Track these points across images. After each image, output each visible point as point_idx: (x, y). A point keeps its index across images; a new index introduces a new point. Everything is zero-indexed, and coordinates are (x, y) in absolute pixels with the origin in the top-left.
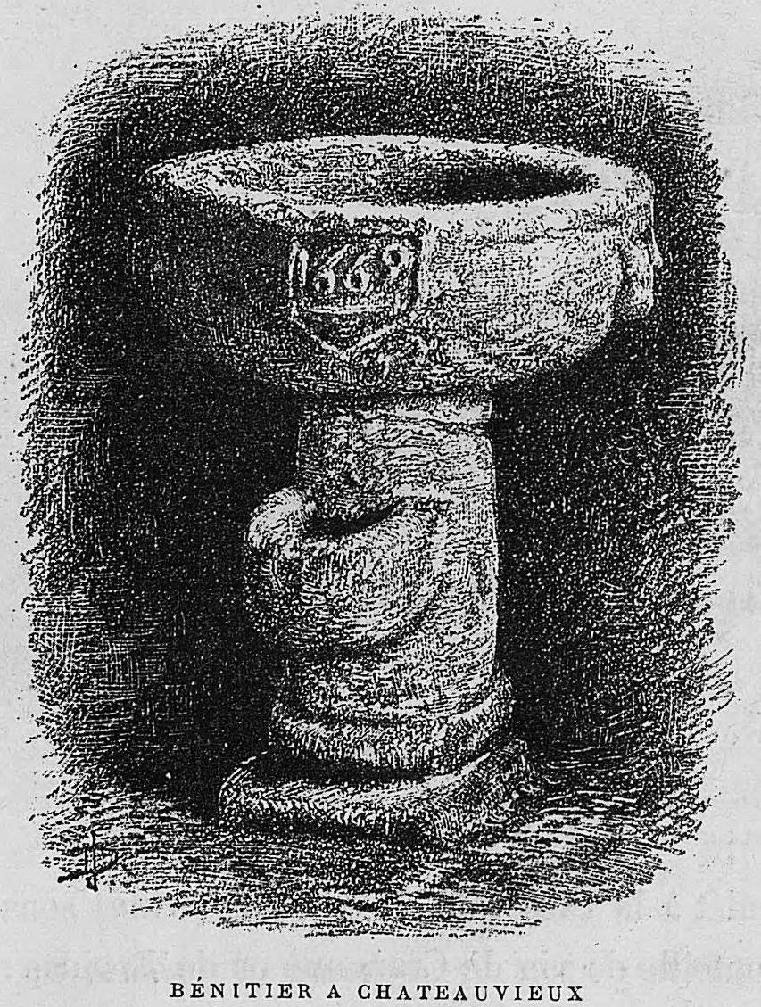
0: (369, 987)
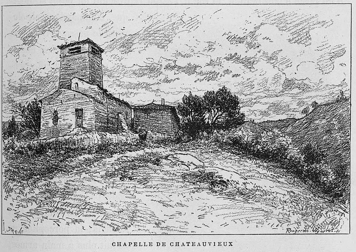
0: (115, 243)
